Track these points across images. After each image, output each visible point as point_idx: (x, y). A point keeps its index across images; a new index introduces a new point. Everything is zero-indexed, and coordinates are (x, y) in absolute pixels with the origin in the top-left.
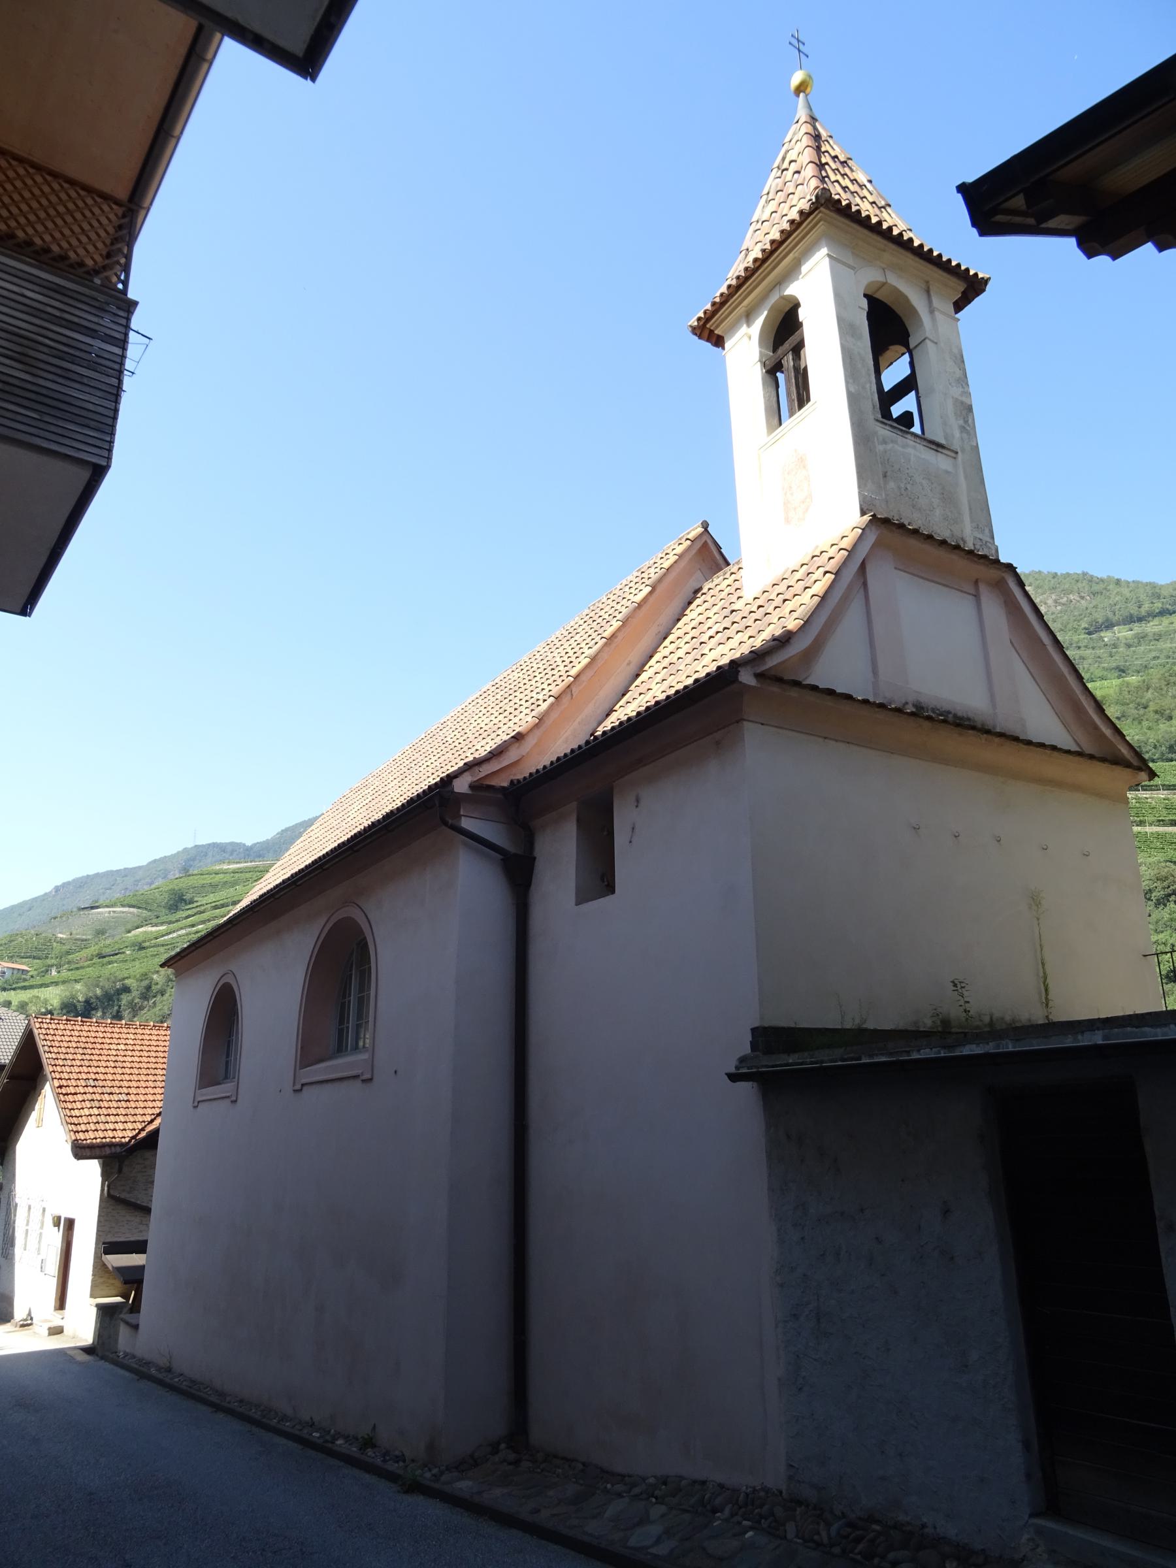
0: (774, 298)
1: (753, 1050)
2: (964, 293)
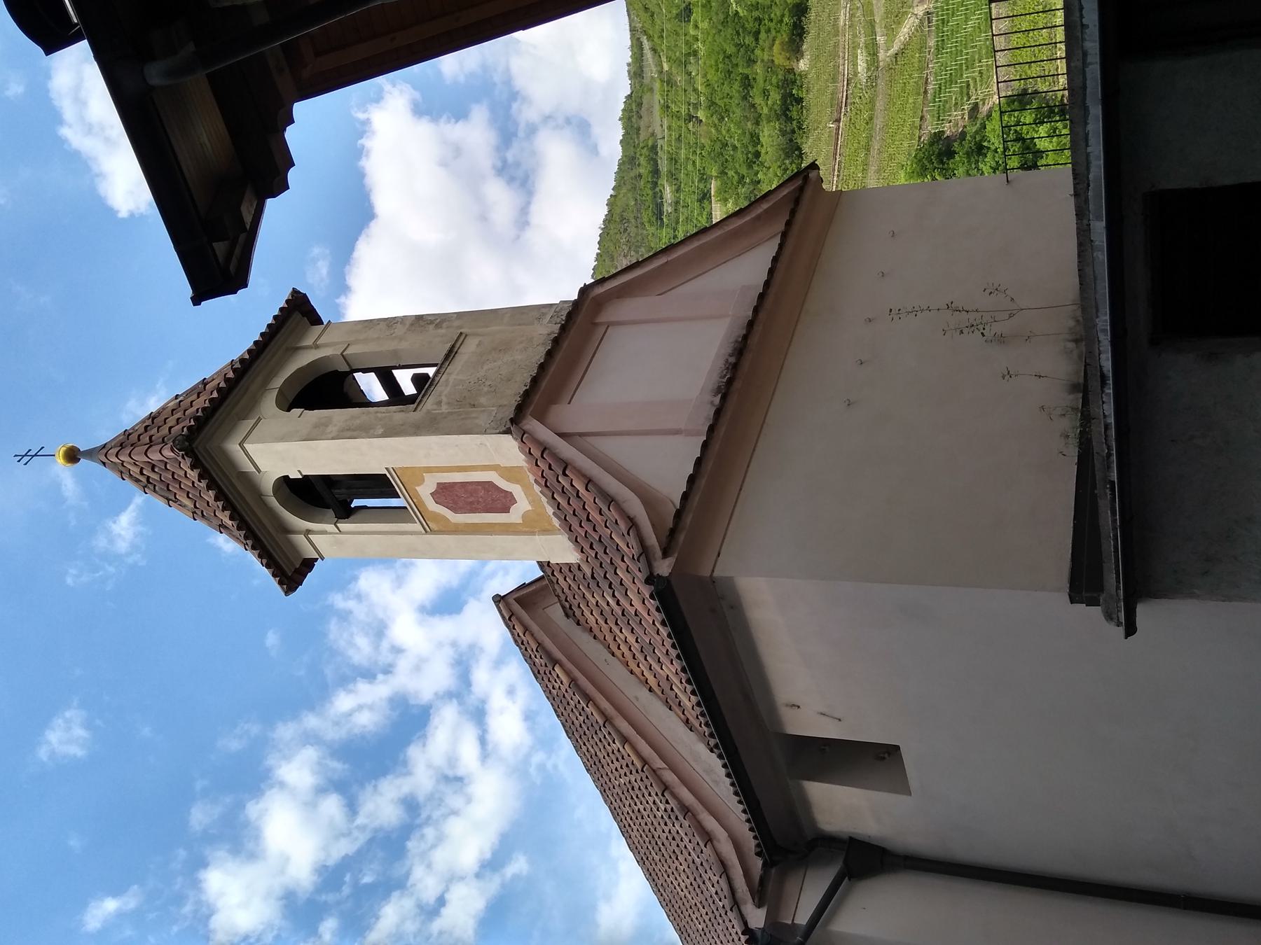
0: (274, 502)
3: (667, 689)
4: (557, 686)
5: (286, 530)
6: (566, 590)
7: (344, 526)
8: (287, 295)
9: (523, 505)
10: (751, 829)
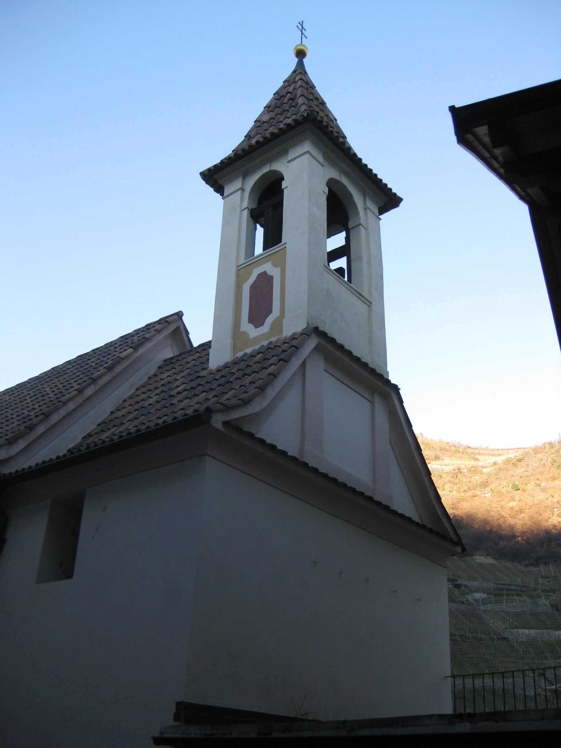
0: (265, 169)
1: (175, 720)
2: (385, 204)
3: (114, 423)
4: (117, 350)
5: (245, 177)
6: (185, 360)
7: (246, 213)
8: (399, 194)
9: (252, 332)
10: (17, 471)
